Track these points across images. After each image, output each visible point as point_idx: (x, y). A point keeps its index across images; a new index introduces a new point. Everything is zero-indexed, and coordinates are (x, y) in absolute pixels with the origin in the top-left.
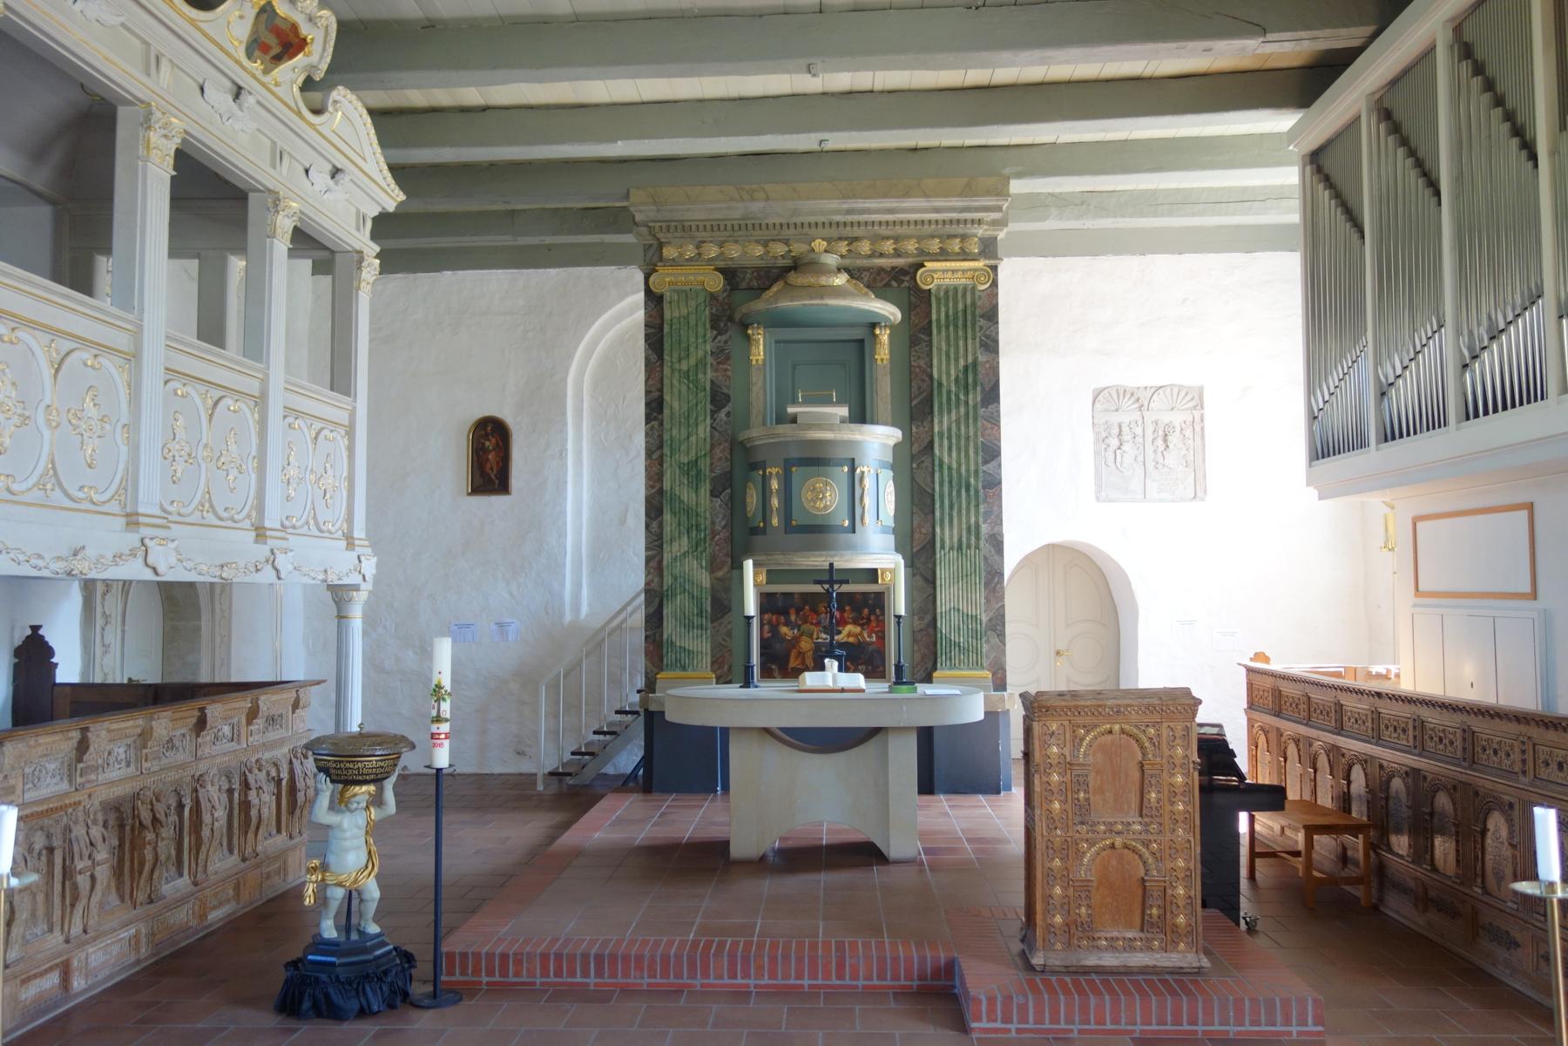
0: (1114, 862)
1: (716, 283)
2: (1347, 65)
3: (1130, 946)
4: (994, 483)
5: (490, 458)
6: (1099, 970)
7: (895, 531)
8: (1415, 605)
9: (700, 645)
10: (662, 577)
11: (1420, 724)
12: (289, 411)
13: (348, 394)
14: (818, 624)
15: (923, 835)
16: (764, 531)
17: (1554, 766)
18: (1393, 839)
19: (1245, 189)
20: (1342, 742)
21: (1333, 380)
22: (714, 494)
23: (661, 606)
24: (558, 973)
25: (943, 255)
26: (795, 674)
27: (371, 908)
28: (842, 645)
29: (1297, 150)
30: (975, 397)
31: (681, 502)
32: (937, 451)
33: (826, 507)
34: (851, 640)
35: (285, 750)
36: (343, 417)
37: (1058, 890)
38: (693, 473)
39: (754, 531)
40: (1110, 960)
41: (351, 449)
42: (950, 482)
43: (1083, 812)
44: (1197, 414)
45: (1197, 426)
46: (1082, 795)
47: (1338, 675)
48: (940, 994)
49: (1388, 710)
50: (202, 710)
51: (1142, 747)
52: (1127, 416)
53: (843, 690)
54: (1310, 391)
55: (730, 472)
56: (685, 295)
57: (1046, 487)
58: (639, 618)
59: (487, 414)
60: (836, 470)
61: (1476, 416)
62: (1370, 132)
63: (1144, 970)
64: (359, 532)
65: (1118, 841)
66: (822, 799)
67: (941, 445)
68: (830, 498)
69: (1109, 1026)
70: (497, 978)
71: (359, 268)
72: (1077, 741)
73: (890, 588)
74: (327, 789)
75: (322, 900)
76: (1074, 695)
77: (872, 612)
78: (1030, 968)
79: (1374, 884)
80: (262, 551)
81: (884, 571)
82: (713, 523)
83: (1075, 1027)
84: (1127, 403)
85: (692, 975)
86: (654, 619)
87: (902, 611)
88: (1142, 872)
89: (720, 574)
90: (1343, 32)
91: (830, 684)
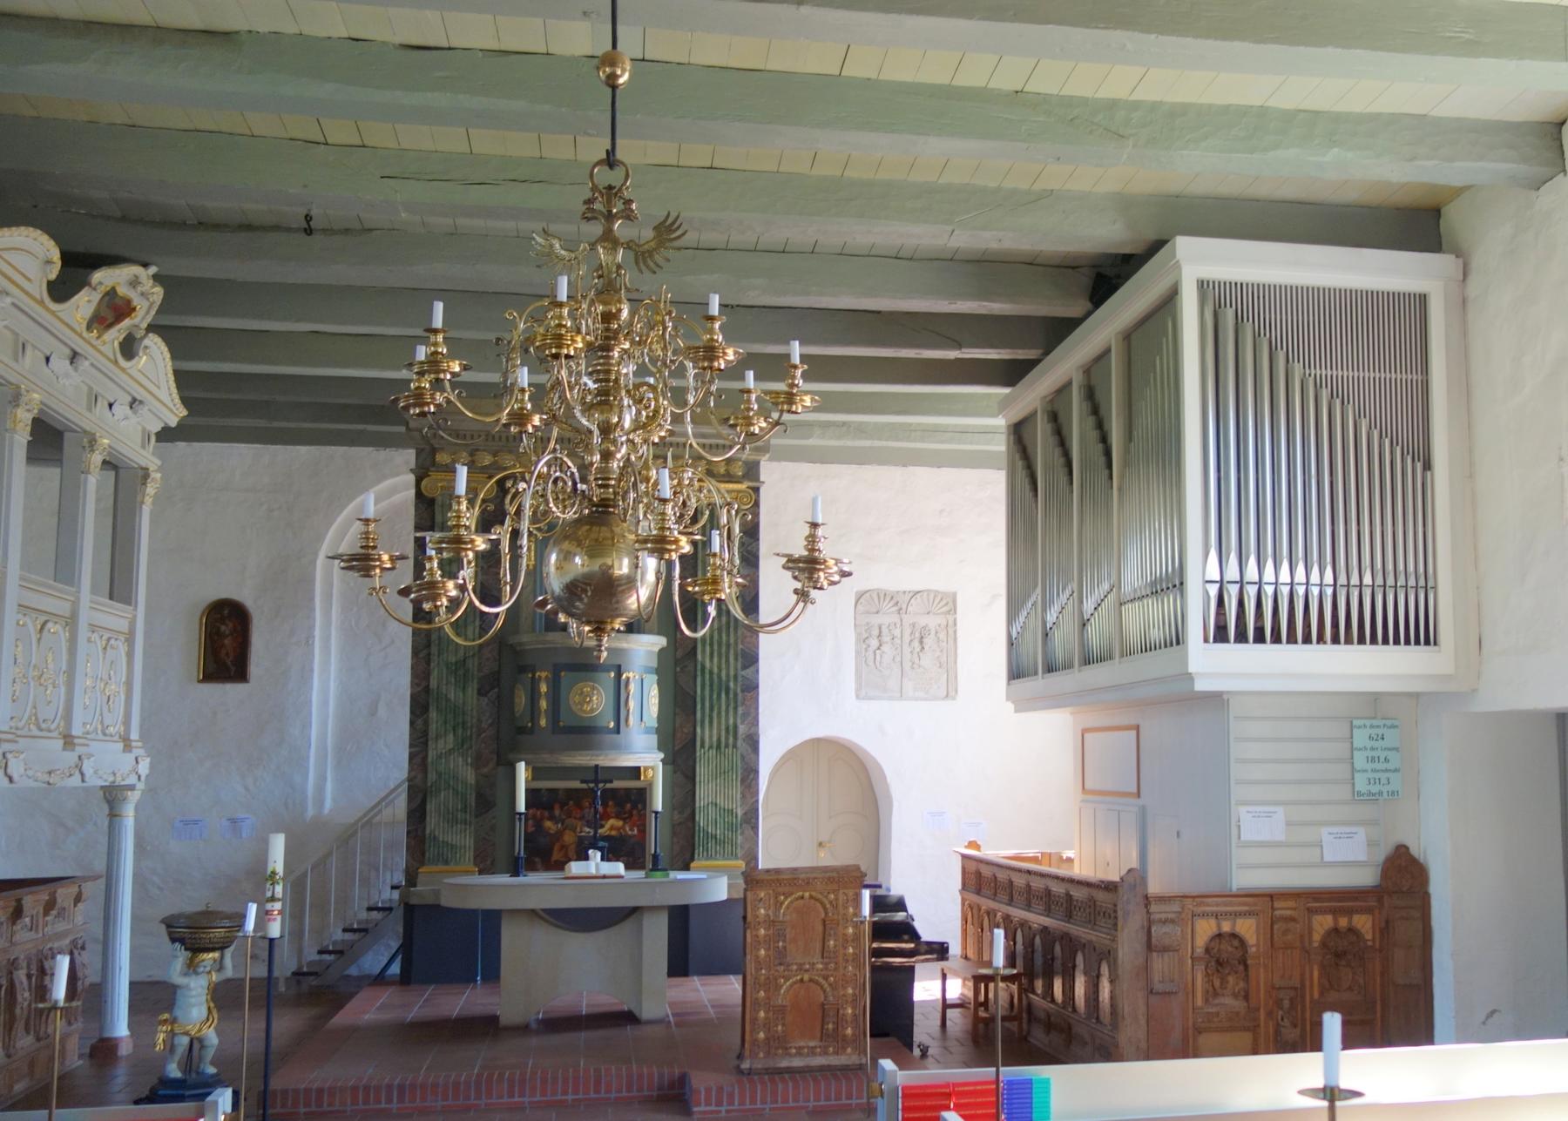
3: (812, 1052)
4: (752, 688)
5: (225, 643)
6: (790, 1070)
7: (658, 731)
9: (464, 840)
10: (425, 772)
12: (93, 628)
13: (129, 604)
14: (582, 818)
15: (672, 1004)
16: (531, 731)
21: (1022, 619)
22: (481, 693)
23: (424, 802)
24: (366, 1102)
26: (560, 866)
27: (210, 1054)
28: (605, 838)
31: (448, 700)
32: (699, 657)
33: (592, 710)
34: (613, 833)
35: (67, 941)
36: (123, 625)
37: (762, 1014)
38: (461, 672)
39: (522, 730)
40: (797, 1063)
41: (130, 655)
42: (711, 686)
43: (781, 957)
45: (951, 630)
47: (1034, 860)
48: (675, 1095)
49: (1078, 894)
50: (19, 901)
52: (887, 618)
53: (604, 877)
55: (499, 672)
57: (804, 685)
59: (224, 596)
60: (603, 675)
64: (134, 735)
65: (806, 977)
66: (580, 974)
67: (704, 651)
68: (598, 702)
69: (792, 1104)
70: (313, 1109)
71: (144, 484)
73: (651, 784)
74: (182, 956)
75: (171, 1047)
76: (778, 871)
77: (634, 807)
78: (740, 1071)
79: (1025, 1021)
80: (70, 757)
81: (646, 769)
82: (479, 721)
83: (767, 1107)
84: (887, 606)
85: (478, 1097)
86: (417, 814)
87: (660, 809)
89: (485, 770)
91: (593, 871)
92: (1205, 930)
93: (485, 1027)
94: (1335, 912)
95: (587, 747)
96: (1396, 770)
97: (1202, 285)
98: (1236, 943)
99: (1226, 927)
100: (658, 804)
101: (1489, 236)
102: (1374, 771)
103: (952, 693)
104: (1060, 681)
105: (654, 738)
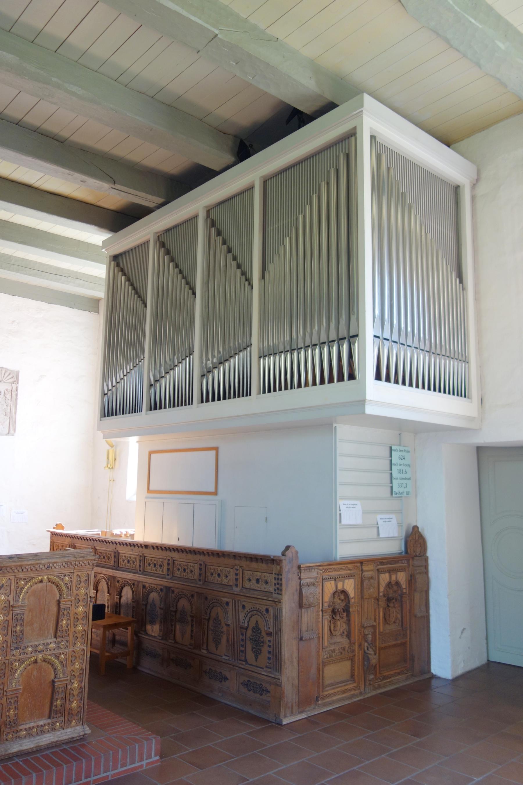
0: (35, 673)
2: (139, 218)
3: (41, 731)
6: (21, 754)
8: (146, 498)
11: (172, 563)
17: (254, 581)
18: (149, 627)
19: (58, 269)
20: (118, 574)
40: (27, 744)
44: (14, 386)
46: (18, 628)
51: (60, 591)
54: (104, 380)
61: (207, 401)
62: (153, 253)
63: (49, 747)
72: (19, 590)
76: (19, 557)
88: (52, 677)
90: (150, 197)
94: (390, 571)
96: (409, 479)
98: (342, 597)
102: (401, 479)
103: (11, 432)
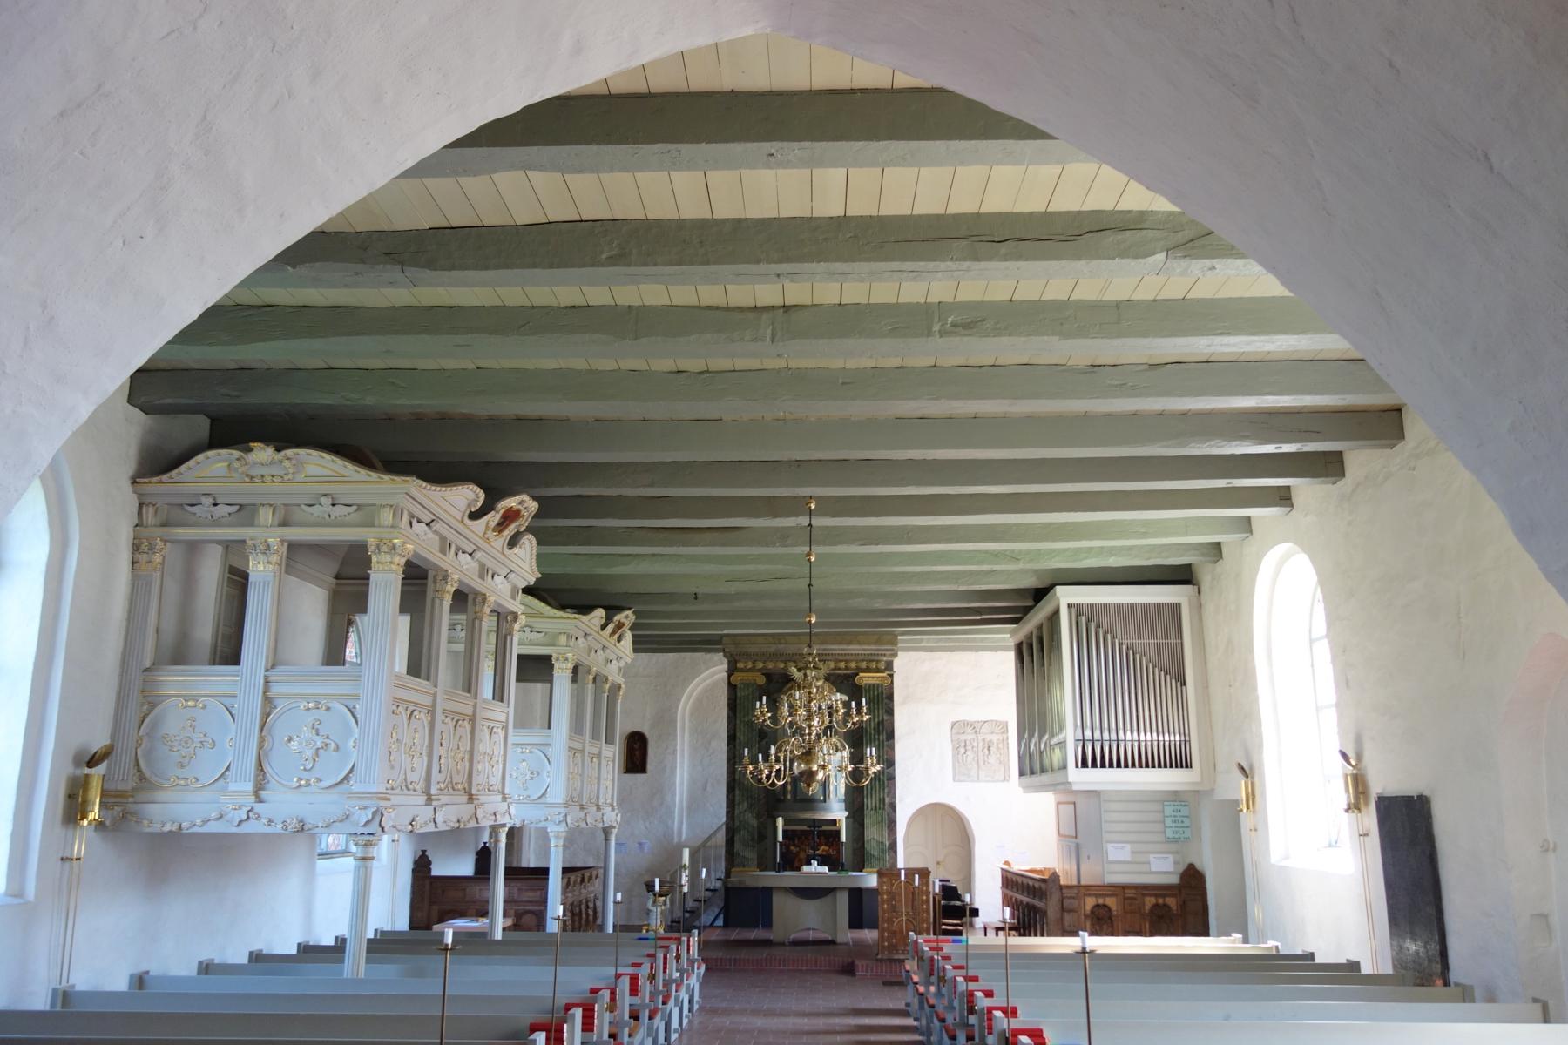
1: (762, 680)
5: (636, 754)
9: (751, 855)
25: (868, 670)
29: (1012, 643)
30: (883, 737)
36: (427, 701)
39: (779, 800)
56: (747, 685)
57: (922, 774)
58: (721, 838)
84: (969, 730)
86: (730, 842)
92: (1090, 903)
93: (767, 943)
94: (1156, 896)
95: (812, 809)
97: (1070, 606)
99: (1101, 901)
100: (844, 839)
101: (1205, 576)
104: (1045, 778)
105: (843, 805)
